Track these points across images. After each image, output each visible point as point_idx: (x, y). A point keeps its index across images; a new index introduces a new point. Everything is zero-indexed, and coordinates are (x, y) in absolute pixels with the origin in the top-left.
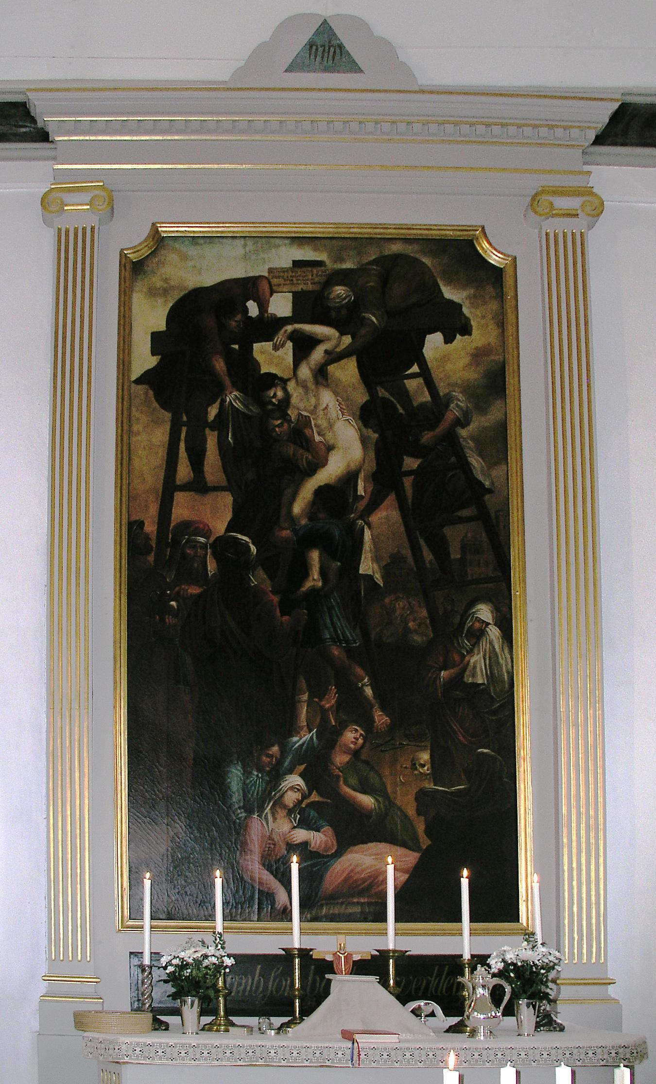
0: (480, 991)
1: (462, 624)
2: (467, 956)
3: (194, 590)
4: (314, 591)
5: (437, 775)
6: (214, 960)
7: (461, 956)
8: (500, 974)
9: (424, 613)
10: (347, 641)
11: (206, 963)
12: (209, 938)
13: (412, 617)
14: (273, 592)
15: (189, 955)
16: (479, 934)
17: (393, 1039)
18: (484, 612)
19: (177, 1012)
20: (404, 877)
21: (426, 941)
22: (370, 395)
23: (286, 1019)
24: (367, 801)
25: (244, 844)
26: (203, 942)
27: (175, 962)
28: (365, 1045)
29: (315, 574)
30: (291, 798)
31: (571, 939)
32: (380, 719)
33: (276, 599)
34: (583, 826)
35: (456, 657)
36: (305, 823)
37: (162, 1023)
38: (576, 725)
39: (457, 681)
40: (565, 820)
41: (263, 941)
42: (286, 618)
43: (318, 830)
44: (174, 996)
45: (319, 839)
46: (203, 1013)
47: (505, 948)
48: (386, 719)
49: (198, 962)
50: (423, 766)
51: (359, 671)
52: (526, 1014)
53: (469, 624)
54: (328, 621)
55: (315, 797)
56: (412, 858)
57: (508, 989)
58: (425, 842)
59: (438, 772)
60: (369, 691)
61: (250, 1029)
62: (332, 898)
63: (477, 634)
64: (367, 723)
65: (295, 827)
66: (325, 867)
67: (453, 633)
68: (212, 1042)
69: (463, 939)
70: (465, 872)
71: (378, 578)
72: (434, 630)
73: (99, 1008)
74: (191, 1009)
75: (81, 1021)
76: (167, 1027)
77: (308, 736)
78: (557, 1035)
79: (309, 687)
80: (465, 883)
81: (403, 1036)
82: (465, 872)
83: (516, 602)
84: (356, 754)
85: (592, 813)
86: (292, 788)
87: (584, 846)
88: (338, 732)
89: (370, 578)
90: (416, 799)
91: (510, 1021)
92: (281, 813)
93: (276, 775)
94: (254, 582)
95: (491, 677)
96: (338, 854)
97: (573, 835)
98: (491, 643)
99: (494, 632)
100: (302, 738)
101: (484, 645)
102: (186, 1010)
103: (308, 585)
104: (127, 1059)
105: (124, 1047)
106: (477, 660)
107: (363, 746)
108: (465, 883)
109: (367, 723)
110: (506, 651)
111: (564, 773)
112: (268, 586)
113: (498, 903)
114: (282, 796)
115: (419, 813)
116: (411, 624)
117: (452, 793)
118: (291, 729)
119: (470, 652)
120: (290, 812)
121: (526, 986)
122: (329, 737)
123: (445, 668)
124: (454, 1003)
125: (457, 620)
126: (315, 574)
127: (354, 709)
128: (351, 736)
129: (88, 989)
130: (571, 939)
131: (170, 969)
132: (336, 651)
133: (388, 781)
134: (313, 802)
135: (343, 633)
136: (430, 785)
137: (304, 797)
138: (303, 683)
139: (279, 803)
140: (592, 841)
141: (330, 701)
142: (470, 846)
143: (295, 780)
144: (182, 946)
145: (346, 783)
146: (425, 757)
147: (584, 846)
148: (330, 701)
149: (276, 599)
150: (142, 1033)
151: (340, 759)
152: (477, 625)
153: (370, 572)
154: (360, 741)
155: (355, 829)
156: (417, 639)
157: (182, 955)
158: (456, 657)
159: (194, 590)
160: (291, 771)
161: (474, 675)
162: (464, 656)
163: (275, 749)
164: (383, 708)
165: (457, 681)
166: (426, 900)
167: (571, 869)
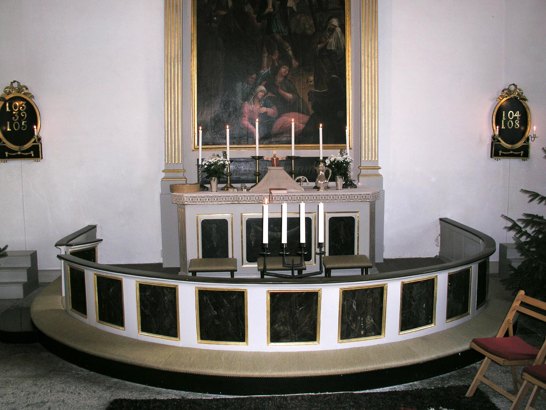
0: (321, 172)
1: (326, 26)
2: (321, 158)
3: (223, 13)
4: (270, 13)
5: (316, 86)
6: (222, 162)
7: (319, 158)
8: (330, 166)
9: (312, 22)
10: (282, 33)
11: (219, 163)
12: (221, 154)
13: (306, 23)
14: (254, 13)
15: (212, 161)
16: (327, 149)
17: (285, 192)
18: (335, 22)
19: (209, 183)
20: (302, 126)
21: (307, 152)
22: (32, 265)
23: (253, 184)
24: (289, 96)
25: (242, 113)
26: (218, 155)
27: (207, 164)
28: (275, 195)
29: (270, 6)
30: (260, 95)
31: (365, 151)
32: (295, 63)
33: (255, 16)
34: (370, 106)
35: (324, 40)
36: (265, 105)
37: (205, 187)
38: (368, 67)
39: (324, 49)
40: (363, 104)
41: (245, 153)
42: (259, 24)
43: (270, 107)
44: (207, 177)
45: (271, 111)
46: (219, 182)
47: (334, 155)
48: (297, 64)
49: (216, 163)
50: (311, 82)
51: (287, 45)
52: (340, 181)
53: (329, 26)
54: (275, 25)
55: (270, 94)
56: (306, 118)
57: (330, 171)
58: (312, 112)
59: (317, 85)
60: (290, 53)
61: (237, 188)
62: (276, 135)
63: (332, 30)
64: (290, 65)
65: (261, 107)
66: (273, 122)
67: (322, 29)
68: (209, 195)
69: (320, 151)
70: (321, 125)
71: (295, 8)
72: (316, 29)
73: (184, 182)
74: (214, 183)
75: (173, 188)
76: (207, 189)
77: (267, 71)
78: (353, 189)
79: (268, 51)
80: (321, 129)
81: (290, 190)
82: (321, 125)
83: (347, 19)
84: (285, 77)
85: (373, 101)
86: (261, 91)
87: (370, 114)
88: (278, 68)
89: (291, 8)
90: (308, 95)
91: (332, 184)
92: (256, 101)
93: (256, 85)
94: (247, 10)
95: (337, 47)
96: (279, 116)
97: (366, 110)
98: (337, 34)
99: (338, 30)
100: (265, 71)
101: (334, 34)
102: (212, 182)
103: (267, 11)
104: (186, 203)
105: (185, 198)
106: (332, 40)
107: (288, 74)
108: (321, 129)
109: (290, 65)
110: (343, 37)
111: (363, 85)
112: (252, 11)
113: (336, 136)
114: (257, 94)
115: (309, 100)
116: (307, 26)
117: (322, 93)
118: (260, 66)
119: (329, 37)
120: (260, 101)
121: (339, 170)
122: (275, 71)
123: (319, 43)
124: (313, 177)
125: (324, 25)
126: (270, 6)
127: (285, 59)
128: (284, 70)
129: (181, 175)
130: (365, 151)
131: (206, 166)
132: (278, 37)
133: (297, 87)
134: (269, 97)
135: (281, 30)
136: (314, 90)
137: (265, 95)
138: (265, 49)
139: (256, 96)
140: (373, 112)
141: (275, 57)
142: (329, 114)
143: (262, 88)
144: (209, 157)
145: (281, 89)
146: (312, 78)
147: (370, 114)
148: (275, 57)
149: (255, 16)
150: (195, 192)
151: (280, 79)
152: (332, 27)
153: (291, 6)
154: (287, 72)
155: (287, 107)
156: (309, 32)
157: (210, 161)
158: (324, 40)
159: (223, 13)
160: (260, 84)
161: (331, 47)
162: (327, 39)
163: (254, 76)
164: (296, 59)
165: (324, 49)
166: (306, 137)
167: (365, 123)
